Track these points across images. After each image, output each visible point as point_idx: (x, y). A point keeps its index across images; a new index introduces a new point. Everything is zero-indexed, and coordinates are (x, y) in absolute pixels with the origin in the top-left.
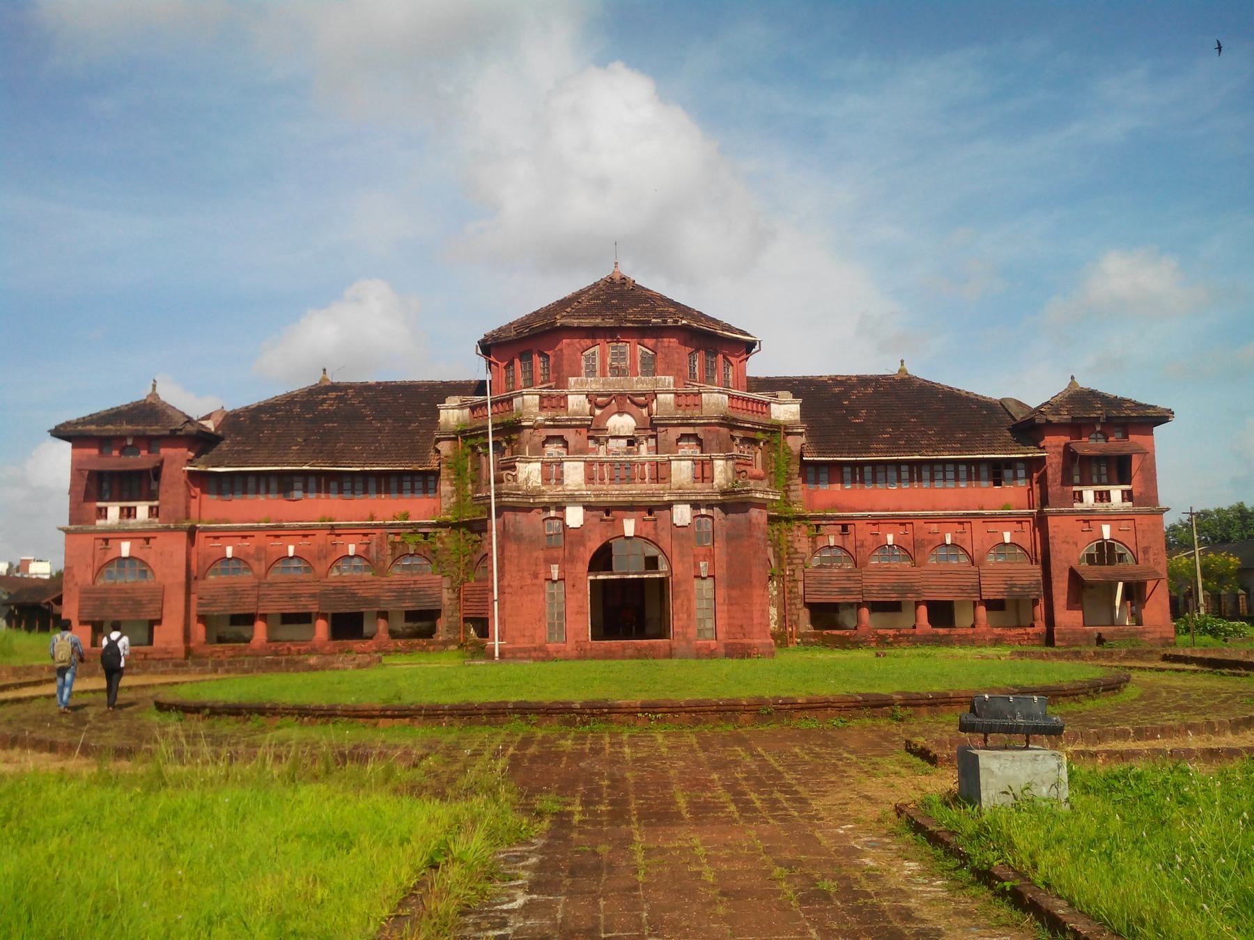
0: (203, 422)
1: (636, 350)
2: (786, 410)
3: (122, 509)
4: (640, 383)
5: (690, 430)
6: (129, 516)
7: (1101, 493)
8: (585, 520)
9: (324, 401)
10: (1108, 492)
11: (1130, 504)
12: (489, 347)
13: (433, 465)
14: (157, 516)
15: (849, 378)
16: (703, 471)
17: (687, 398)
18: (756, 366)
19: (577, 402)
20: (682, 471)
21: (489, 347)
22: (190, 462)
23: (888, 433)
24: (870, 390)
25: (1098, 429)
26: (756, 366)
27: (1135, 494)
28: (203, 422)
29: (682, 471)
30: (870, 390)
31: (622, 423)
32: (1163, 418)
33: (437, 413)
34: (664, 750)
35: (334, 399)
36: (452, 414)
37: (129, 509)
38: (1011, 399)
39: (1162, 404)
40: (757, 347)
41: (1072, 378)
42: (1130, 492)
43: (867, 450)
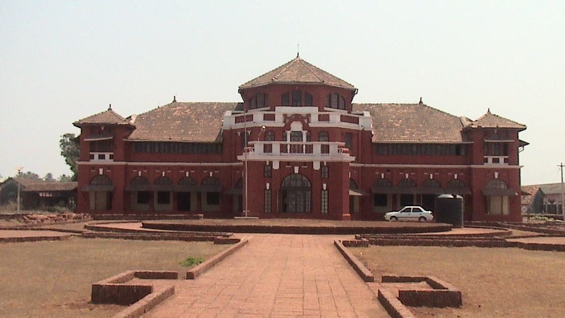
9: (175, 111)
21: (242, 91)
35: (179, 110)
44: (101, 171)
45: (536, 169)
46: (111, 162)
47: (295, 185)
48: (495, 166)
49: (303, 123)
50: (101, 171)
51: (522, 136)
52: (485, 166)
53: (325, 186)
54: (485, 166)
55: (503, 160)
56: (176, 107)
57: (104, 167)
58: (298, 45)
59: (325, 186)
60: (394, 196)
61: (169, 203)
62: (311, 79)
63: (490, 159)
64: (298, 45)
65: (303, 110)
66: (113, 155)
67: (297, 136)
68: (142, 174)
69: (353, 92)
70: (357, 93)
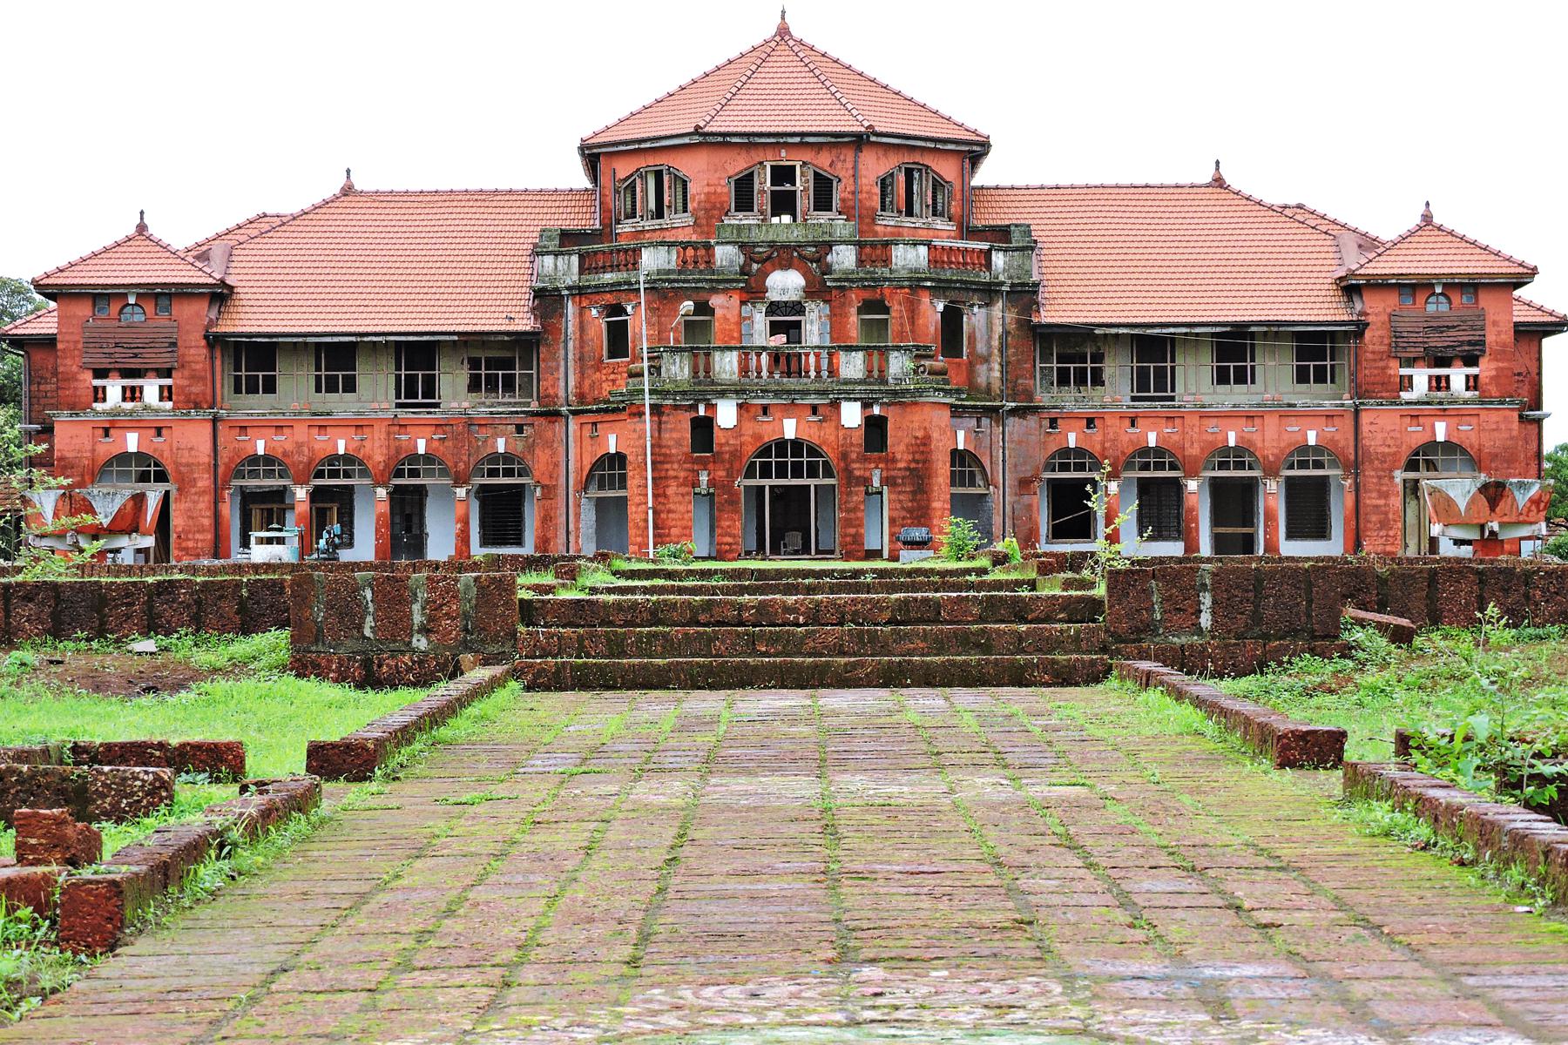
39: (1531, 262)
69: (974, 152)
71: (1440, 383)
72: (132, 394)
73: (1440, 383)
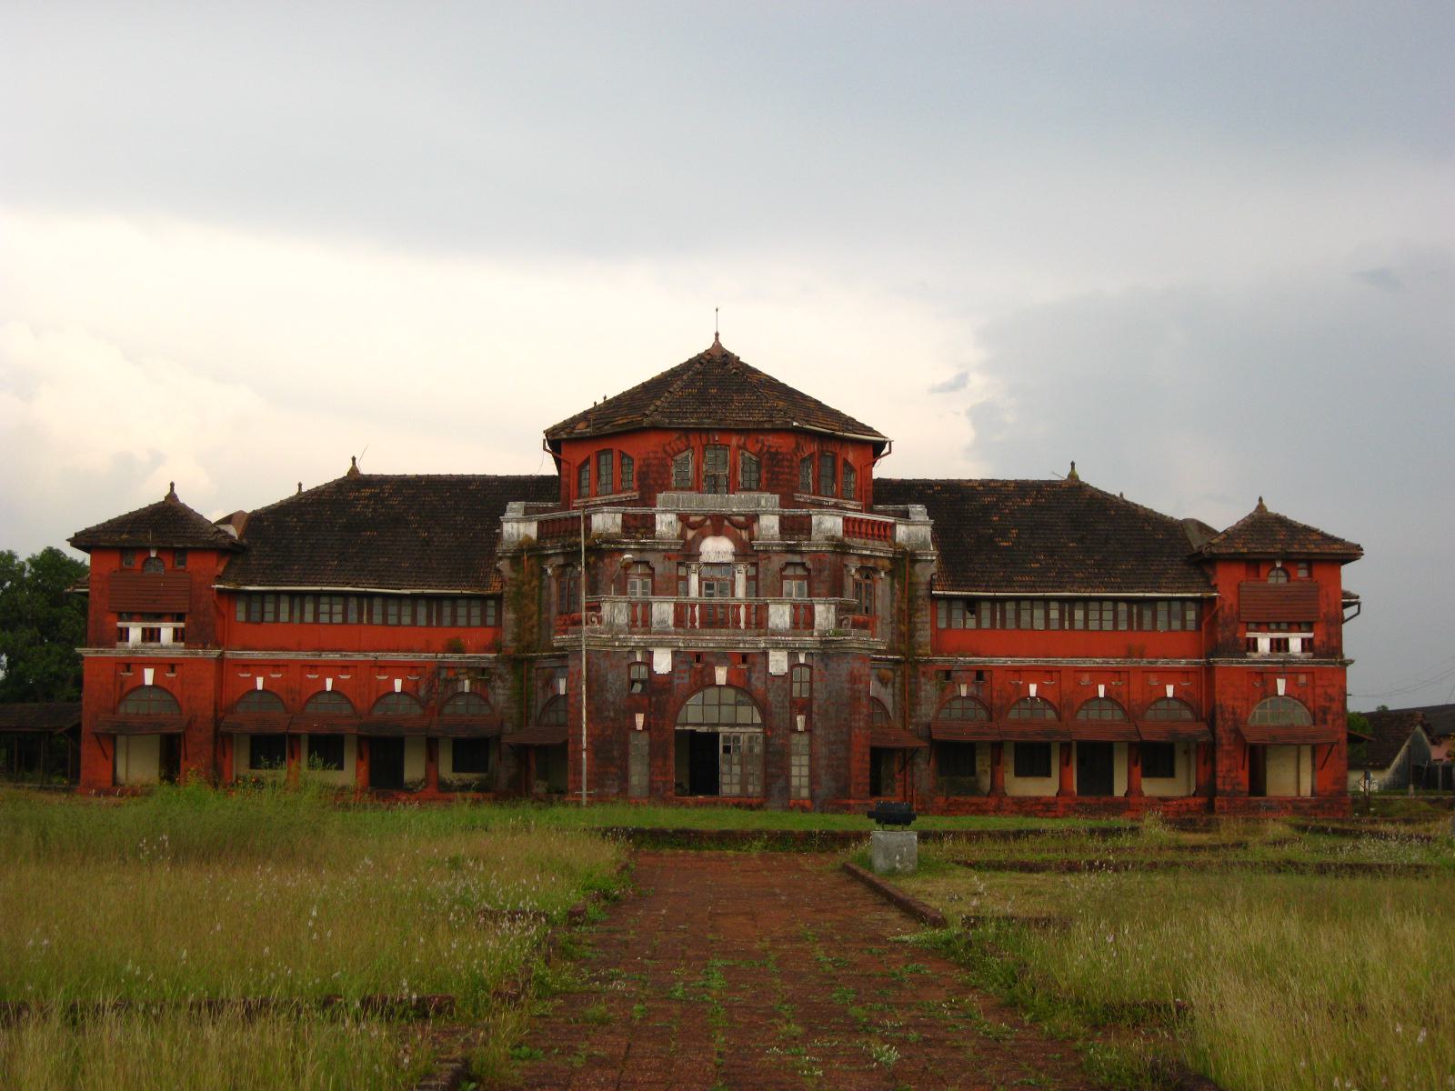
0: (223, 527)
1: (741, 454)
2: (915, 529)
3: (144, 630)
4: (736, 503)
5: (797, 559)
6: (151, 640)
7: (1279, 640)
8: (673, 667)
10: (1286, 641)
11: (1311, 654)
12: (558, 440)
13: (495, 588)
14: (183, 640)
15: (1005, 483)
16: (803, 619)
17: (795, 527)
18: (884, 469)
19: (665, 523)
20: (780, 616)
22: (219, 579)
23: (1038, 561)
24: (1028, 502)
25: (1279, 565)
26: (884, 469)
27: (1317, 643)
28: (223, 527)
29: (780, 616)
30: (1028, 502)
31: (717, 548)
32: (1351, 553)
33: (500, 525)
34: (828, 968)
35: (369, 498)
36: (517, 527)
37: (152, 630)
38: (1193, 521)
39: (1350, 537)
40: (886, 450)
41: (1261, 499)
42: (1310, 640)
43: (1009, 584)
44: (149, 676)
45: (1386, 666)
46: (179, 651)
47: (1110, 718)
48: (152, 650)
49: (737, 541)
50: (149, 676)
51: (1351, 577)
52: (119, 651)
53: (640, 719)
54: (119, 651)
55: (1299, 641)
56: (359, 491)
57: (160, 665)
58: (717, 310)
59: (640, 719)
60: (997, 748)
61: (453, 771)
62: (1337, 548)
63: (135, 633)
64: (717, 310)
65: (736, 503)
66: (182, 629)
67: (716, 578)
68: (403, 685)
69: (877, 447)
70: (890, 452)
71: (1279, 646)
72: (151, 636)
73: (1279, 646)
